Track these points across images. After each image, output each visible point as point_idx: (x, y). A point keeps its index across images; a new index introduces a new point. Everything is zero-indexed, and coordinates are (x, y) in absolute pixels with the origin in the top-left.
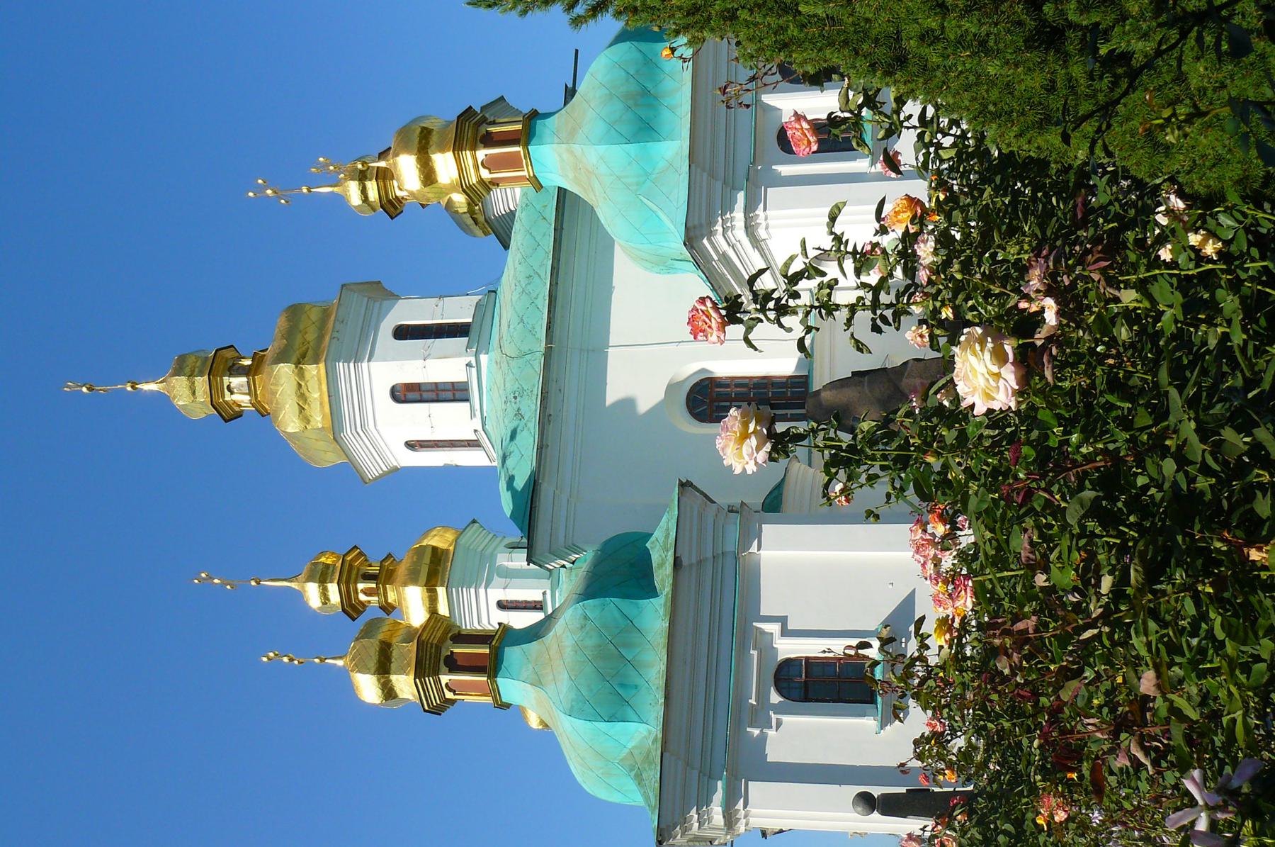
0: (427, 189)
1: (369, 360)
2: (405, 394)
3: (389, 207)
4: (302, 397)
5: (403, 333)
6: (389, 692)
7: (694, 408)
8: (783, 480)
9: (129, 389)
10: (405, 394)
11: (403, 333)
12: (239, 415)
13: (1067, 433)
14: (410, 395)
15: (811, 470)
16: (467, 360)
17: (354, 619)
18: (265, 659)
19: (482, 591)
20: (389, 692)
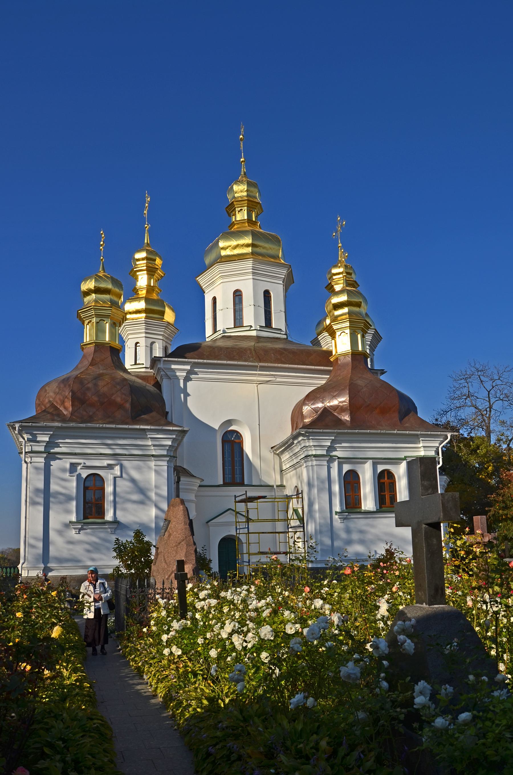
0: (331, 305)
1: (253, 279)
2: (238, 295)
3: (330, 286)
4: (243, 246)
5: (267, 294)
6: (87, 293)
7: (237, 435)
8: (194, 476)
9: (242, 160)
10: (238, 295)
11: (267, 294)
12: (229, 215)
13: (65, 606)
14: (237, 299)
15: (196, 488)
16: (253, 326)
17: (326, 287)
18: (102, 232)
19: (161, 337)
20: (87, 293)
